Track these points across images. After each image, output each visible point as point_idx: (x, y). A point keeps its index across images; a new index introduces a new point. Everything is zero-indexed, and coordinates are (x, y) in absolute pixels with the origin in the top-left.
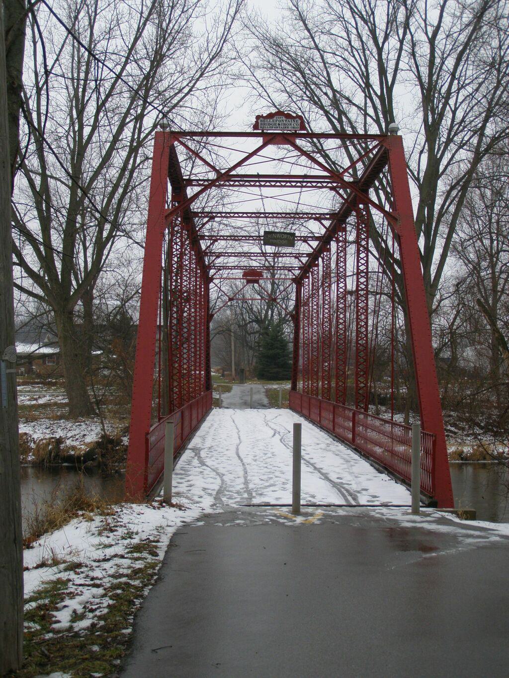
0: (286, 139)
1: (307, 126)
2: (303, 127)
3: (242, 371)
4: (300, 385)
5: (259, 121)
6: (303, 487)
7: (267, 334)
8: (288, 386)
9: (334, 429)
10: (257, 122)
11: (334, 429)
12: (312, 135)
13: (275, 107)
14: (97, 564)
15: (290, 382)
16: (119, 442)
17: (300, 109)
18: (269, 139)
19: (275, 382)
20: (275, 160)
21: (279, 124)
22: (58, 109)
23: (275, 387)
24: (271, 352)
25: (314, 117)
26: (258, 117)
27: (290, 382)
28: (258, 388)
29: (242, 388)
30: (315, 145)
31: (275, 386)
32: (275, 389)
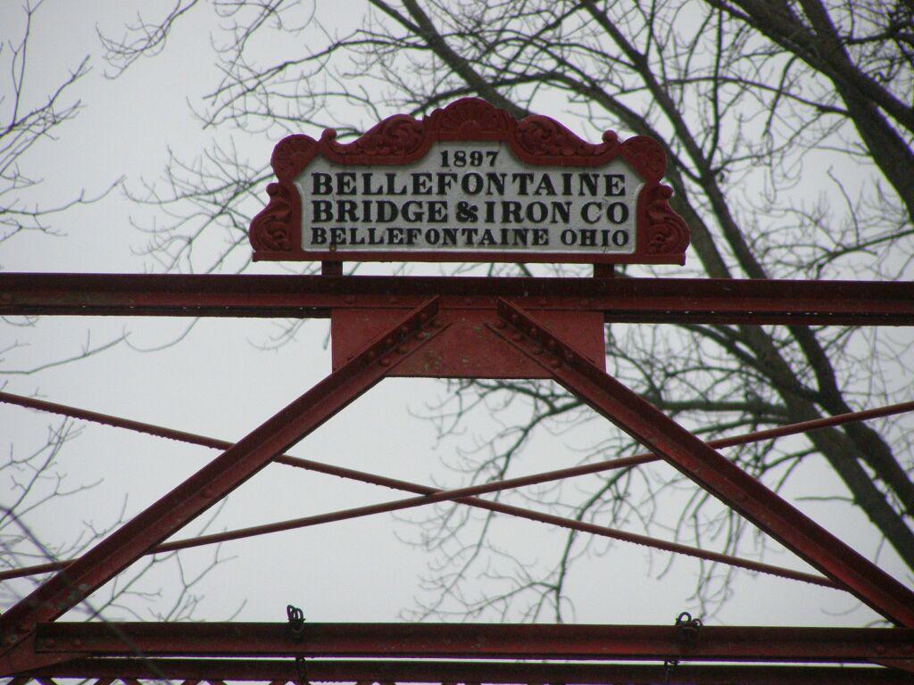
0: (523, 325)
1: (698, 199)
2: (666, 228)
5: (304, 186)
10: (283, 194)
12: (742, 304)
13: (436, 43)
14: (315, 64)
17: (639, 63)
18: (388, 334)
20: (430, 496)
21: (466, 212)
25: (753, 131)
26: (292, 154)
30: (770, 365)
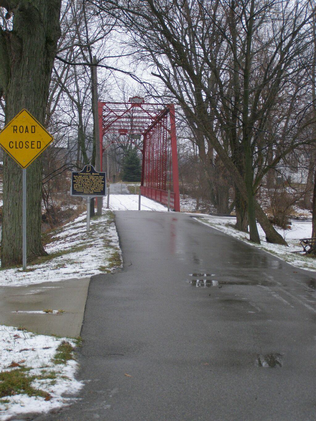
3: (114, 176)
4: (145, 185)
6: (141, 203)
7: (128, 155)
8: (139, 185)
9: (161, 201)
11: (161, 201)
15: (141, 182)
16: (59, 209)
19: (133, 183)
22: (68, 113)
23: (133, 185)
24: (131, 166)
27: (141, 182)
28: (125, 185)
29: (115, 185)
31: (133, 185)
32: (133, 186)
